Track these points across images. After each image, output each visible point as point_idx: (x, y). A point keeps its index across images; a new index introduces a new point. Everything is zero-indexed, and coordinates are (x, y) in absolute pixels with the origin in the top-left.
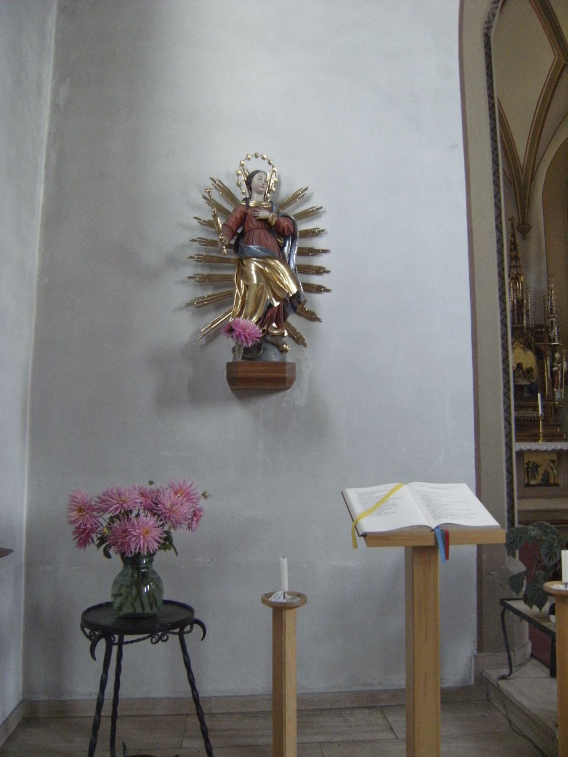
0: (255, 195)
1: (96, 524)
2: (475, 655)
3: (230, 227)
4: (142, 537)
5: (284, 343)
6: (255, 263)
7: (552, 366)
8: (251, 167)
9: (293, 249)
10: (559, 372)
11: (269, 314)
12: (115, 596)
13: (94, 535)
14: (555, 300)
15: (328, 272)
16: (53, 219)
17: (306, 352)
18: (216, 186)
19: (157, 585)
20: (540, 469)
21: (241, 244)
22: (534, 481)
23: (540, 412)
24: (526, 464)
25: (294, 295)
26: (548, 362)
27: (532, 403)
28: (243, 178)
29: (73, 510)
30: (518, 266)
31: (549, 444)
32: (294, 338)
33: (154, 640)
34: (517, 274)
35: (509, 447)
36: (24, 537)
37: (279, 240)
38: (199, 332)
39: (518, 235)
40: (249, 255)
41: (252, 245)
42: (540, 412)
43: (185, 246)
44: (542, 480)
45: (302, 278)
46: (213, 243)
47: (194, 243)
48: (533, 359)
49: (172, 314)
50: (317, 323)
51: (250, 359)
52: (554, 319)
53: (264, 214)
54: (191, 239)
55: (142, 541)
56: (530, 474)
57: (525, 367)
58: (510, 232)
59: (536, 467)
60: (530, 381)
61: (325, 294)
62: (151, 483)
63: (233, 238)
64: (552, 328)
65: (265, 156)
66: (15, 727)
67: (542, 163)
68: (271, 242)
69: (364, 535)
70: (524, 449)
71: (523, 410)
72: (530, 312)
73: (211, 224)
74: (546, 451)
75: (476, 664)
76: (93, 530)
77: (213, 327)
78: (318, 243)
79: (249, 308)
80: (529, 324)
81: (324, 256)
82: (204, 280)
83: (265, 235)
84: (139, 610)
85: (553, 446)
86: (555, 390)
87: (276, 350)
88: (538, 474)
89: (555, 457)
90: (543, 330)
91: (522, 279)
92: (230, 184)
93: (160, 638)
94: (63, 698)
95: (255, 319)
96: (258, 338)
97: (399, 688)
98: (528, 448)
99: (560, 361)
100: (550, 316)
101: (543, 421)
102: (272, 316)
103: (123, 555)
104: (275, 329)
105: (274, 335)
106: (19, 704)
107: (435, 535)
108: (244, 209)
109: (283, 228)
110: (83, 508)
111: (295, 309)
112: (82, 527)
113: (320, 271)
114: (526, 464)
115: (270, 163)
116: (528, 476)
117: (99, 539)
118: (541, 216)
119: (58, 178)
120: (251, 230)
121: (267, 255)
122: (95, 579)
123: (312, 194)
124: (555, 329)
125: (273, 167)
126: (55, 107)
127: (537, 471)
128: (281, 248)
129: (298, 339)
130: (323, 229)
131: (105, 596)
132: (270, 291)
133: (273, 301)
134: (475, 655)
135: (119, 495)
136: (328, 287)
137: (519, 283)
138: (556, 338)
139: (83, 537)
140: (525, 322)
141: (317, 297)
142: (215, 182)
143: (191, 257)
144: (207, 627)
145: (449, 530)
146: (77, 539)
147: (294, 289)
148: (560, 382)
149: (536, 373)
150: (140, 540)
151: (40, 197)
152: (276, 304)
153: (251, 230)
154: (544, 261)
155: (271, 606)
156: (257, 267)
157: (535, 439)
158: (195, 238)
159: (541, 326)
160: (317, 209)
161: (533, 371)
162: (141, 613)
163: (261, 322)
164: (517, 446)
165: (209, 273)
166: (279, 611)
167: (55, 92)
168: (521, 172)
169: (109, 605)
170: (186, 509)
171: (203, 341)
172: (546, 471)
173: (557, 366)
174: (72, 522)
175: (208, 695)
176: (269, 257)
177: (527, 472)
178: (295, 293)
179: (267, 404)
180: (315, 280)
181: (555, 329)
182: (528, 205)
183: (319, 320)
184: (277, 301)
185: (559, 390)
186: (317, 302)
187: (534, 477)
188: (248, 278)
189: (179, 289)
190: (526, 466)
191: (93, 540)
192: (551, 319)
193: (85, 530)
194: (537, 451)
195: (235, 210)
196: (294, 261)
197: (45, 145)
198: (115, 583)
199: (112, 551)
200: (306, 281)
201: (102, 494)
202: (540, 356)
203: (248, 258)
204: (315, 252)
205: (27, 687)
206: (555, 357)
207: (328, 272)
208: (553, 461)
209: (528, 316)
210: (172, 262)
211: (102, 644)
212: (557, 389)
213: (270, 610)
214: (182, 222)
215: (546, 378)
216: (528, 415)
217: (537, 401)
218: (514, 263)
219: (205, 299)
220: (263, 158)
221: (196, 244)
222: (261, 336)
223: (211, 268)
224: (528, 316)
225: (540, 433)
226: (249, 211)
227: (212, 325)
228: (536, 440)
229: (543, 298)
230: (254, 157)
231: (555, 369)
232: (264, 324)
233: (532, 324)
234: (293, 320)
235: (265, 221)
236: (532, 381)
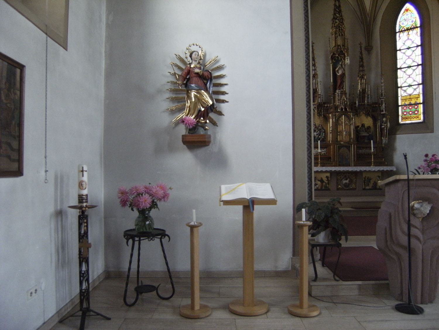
0: (193, 62)
1: (128, 199)
2: (291, 258)
3: (183, 76)
4: (143, 202)
5: (206, 126)
6: (193, 92)
7: (381, 125)
8: (193, 48)
9: (211, 85)
10: (385, 128)
11: (200, 114)
12: (136, 225)
13: (127, 203)
14: (384, 89)
15: (227, 94)
16: (109, 75)
17: (218, 129)
18: (178, 58)
19: (151, 221)
20: (371, 181)
21: (188, 83)
22: (368, 187)
23: (372, 150)
24: (364, 178)
25: (211, 105)
26: (379, 123)
27: (184, 100)
28: (188, 55)
29: (119, 193)
30: (363, 70)
31: (376, 167)
32: (212, 123)
33: (149, 240)
34: (363, 75)
35: (310, 169)
36: (103, 209)
37: (205, 81)
38: (171, 122)
39: (364, 53)
40: (191, 89)
41: (192, 84)
42: (372, 150)
43: (165, 84)
44: (372, 186)
45: (215, 97)
46: (176, 83)
47: (169, 83)
48: (371, 121)
49: (161, 114)
50: (223, 116)
51: (191, 133)
52: (383, 100)
53: (197, 70)
54: (167, 82)
55: (144, 204)
56: (366, 183)
57: (366, 126)
58: (360, 51)
59: (369, 179)
60: (368, 133)
61: (226, 104)
62: (150, 184)
63: (184, 80)
64: (382, 104)
65: (197, 44)
66: (102, 279)
67: (380, 10)
68: (200, 82)
69: (222, 201)
70: (362, 170)
71: (364, 149)
72: (369, 96)
73: (175, 74)
74: (374, 171)
75: (292, 261)
76: (127, 201)
77: (177, 119)
78: (222, 81)
79: (192, 111)
80: (369, 103)
81: (226, 86)
82: (173, 100)
83: (198, 80)
84: (145, 230)
85: (378, 168)
86: (383, 138)
87: (203, 129)
88: (370, 183)
89: (328, 175)
90: (377, 105)
91: (365, 78)
92: (183, 56)
93: (151, 239)
94: (120, 270)
95: (193, 116)
96: (194, 125)
97: (258, 270)
98: (365, 169)
99: (386, 123)
100: (381, 97)
101: (374, 155)
102: (201, 114)
103: (138, 209)
104: (203, 120)
105: (202, 123)
106: (104, 272)
107: (249, 202)
108: (189, 69)
109: (206, 76)
110: (123, 193)
111: (212, 111)
112: (123, 199)
113: (224, 93)
114: (364, 178)
115: (200, 47)
116: (365, 185)
117: (130, 204)
118: (379, 42)
119: (110, 56)
120: (192, 77)
121: (198, 89)
122: (129, 219)
123: (220, 59)
124: (384, 104)
125: (202, 49)
126: (108, 25)
127: (370, 182)
128: (206, 85)
129: (214, 123)
130: (225, 74)
131: (133, 227)
132: (200, 104)
133: (201, 108)
134: (291, 258)
135: (136, 188)
136: (227, 100)
137: (364, 80)
138: (384, 110)
139: (124, 203)
140: (366, 101)
141: (223, 105)
142: (177, 56)
143: (168, 90)
144: (170, 237)
145: (254, 199)
146: (121, 204)
147: (211, 103)
148: (385, 134)
149: (372, 129)
150: (143, 203)
151: (103, 66)
152: (203, 109)
153: (192, 77)
154: (380, 66)
155: (189, 226)
156: (195, 95)
157: (369, 165)
158: (169, 81)
159: (376, 103)
160: (222, 66)
161: (370, 128)
162: (145, 230)
163: (196, 117)
164: (314, 169)
165: (175, 96)
166: (192, 228)
167: (107, 19)
168: (367, 16)
169: (134, 230)
170: (161, 193)
171: (174, 125)
172: (375, 182)
173: (384, 125)
174: (119, 198)
175: (178, 270)
176: (199, 90)
177: (364, 182)
178: (211, 104)
179: (201, 151)
180: (222, 97)
181: (384, 104)
182: (372, 34)
183: (223, 115)
184: (203, 108)
185: (385, 138)
186: (223, 107)
187: (368, 185)
188: (191, 99)
189: (163, 103)
190: (364, 179)
191: (127, 204)
192: (381, 99)
193: (124, 200)
194: (370, 171)
195: (185, 68)
196: (211, 89)
197: (104, 43)
198: (136, 220)
199: (134, 209)
200: (215, 98)
201: (425, 309)
202: (375, 120)
203: (191, 90)
204: (221, 85)
205: (106, 266)
206: (383, 121)
207: (227, 94)
208: (379, 177)
209: (368, 98)
210: (160, 91)
211: (131, 241)
212: (384, 138)
213: (189, 229)
214: (164, 74)
215: (378, 132)
216: (367, 152)
217: (371, 144)
218: (361, 68)
219: (174, 108)
220: (197, 45)
221: (169, 84)
222: (196, 123)
223: (176, 94)
224: (368, 98)
225: (372, 161)
226: (191, 69)
227: (177, 118)
228: (370, 166)
229: (377, 88)
230: (193, 45)
231: (383, 127)
232: (198, 119)
233: (370, 102)
234: (212, 115)
235: (197, 73)
236: (370, 133)
